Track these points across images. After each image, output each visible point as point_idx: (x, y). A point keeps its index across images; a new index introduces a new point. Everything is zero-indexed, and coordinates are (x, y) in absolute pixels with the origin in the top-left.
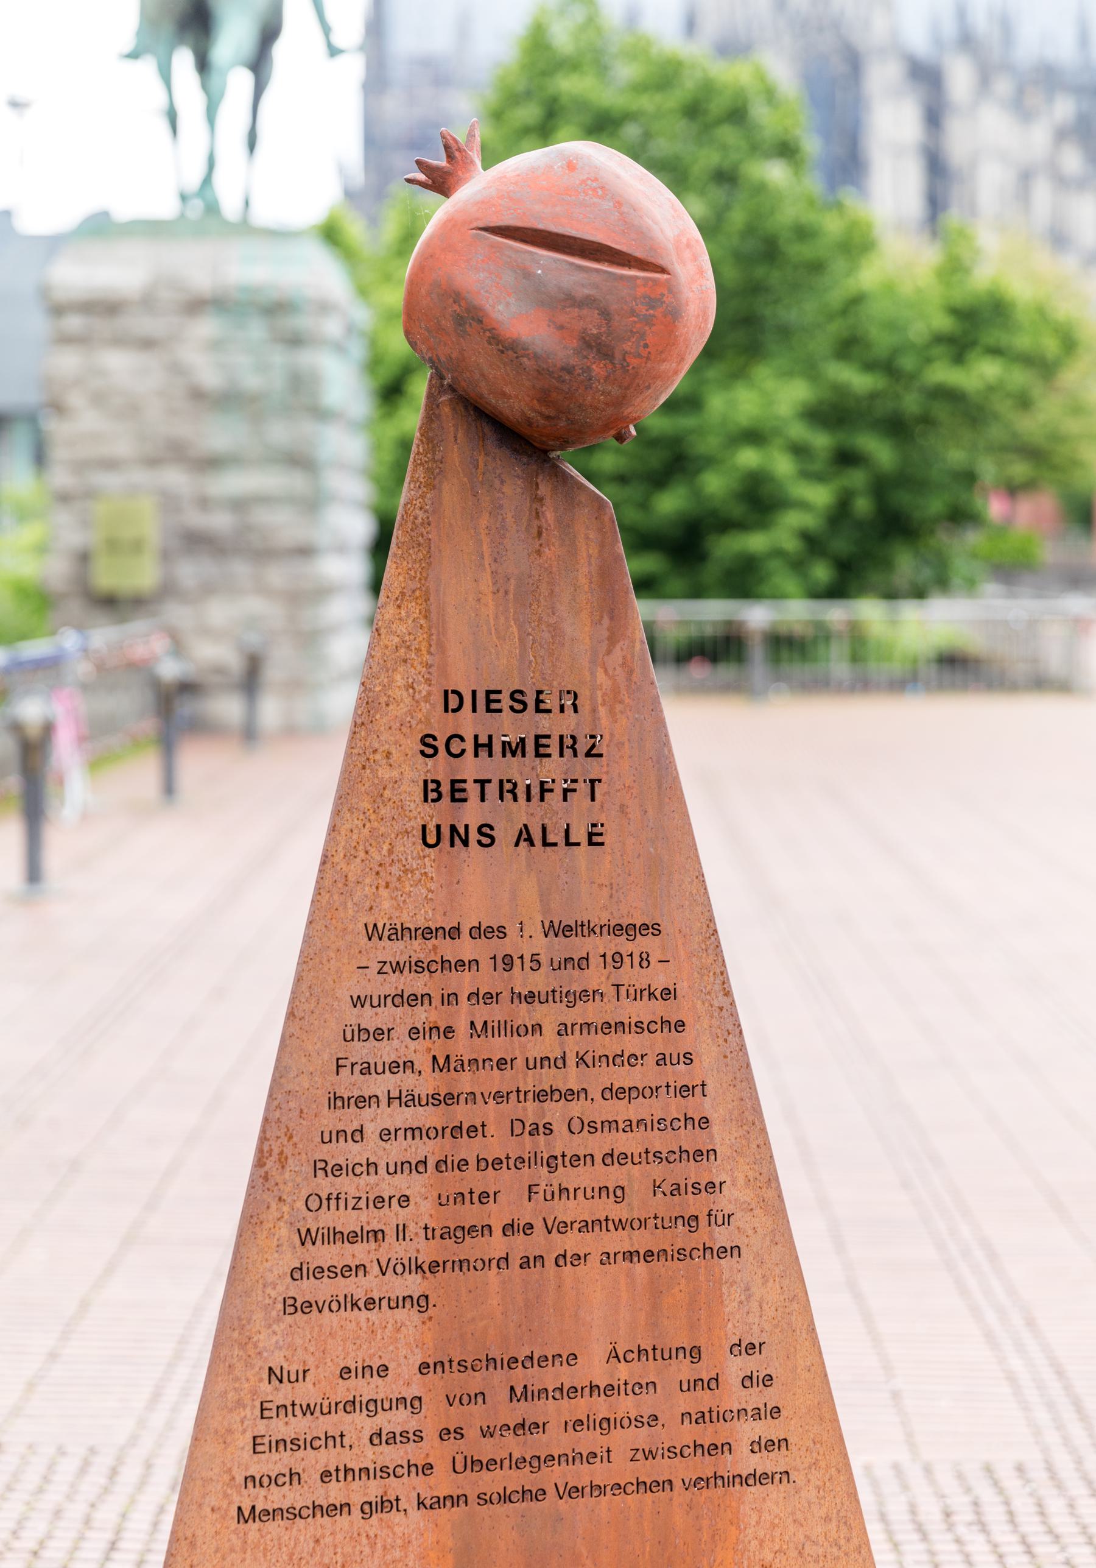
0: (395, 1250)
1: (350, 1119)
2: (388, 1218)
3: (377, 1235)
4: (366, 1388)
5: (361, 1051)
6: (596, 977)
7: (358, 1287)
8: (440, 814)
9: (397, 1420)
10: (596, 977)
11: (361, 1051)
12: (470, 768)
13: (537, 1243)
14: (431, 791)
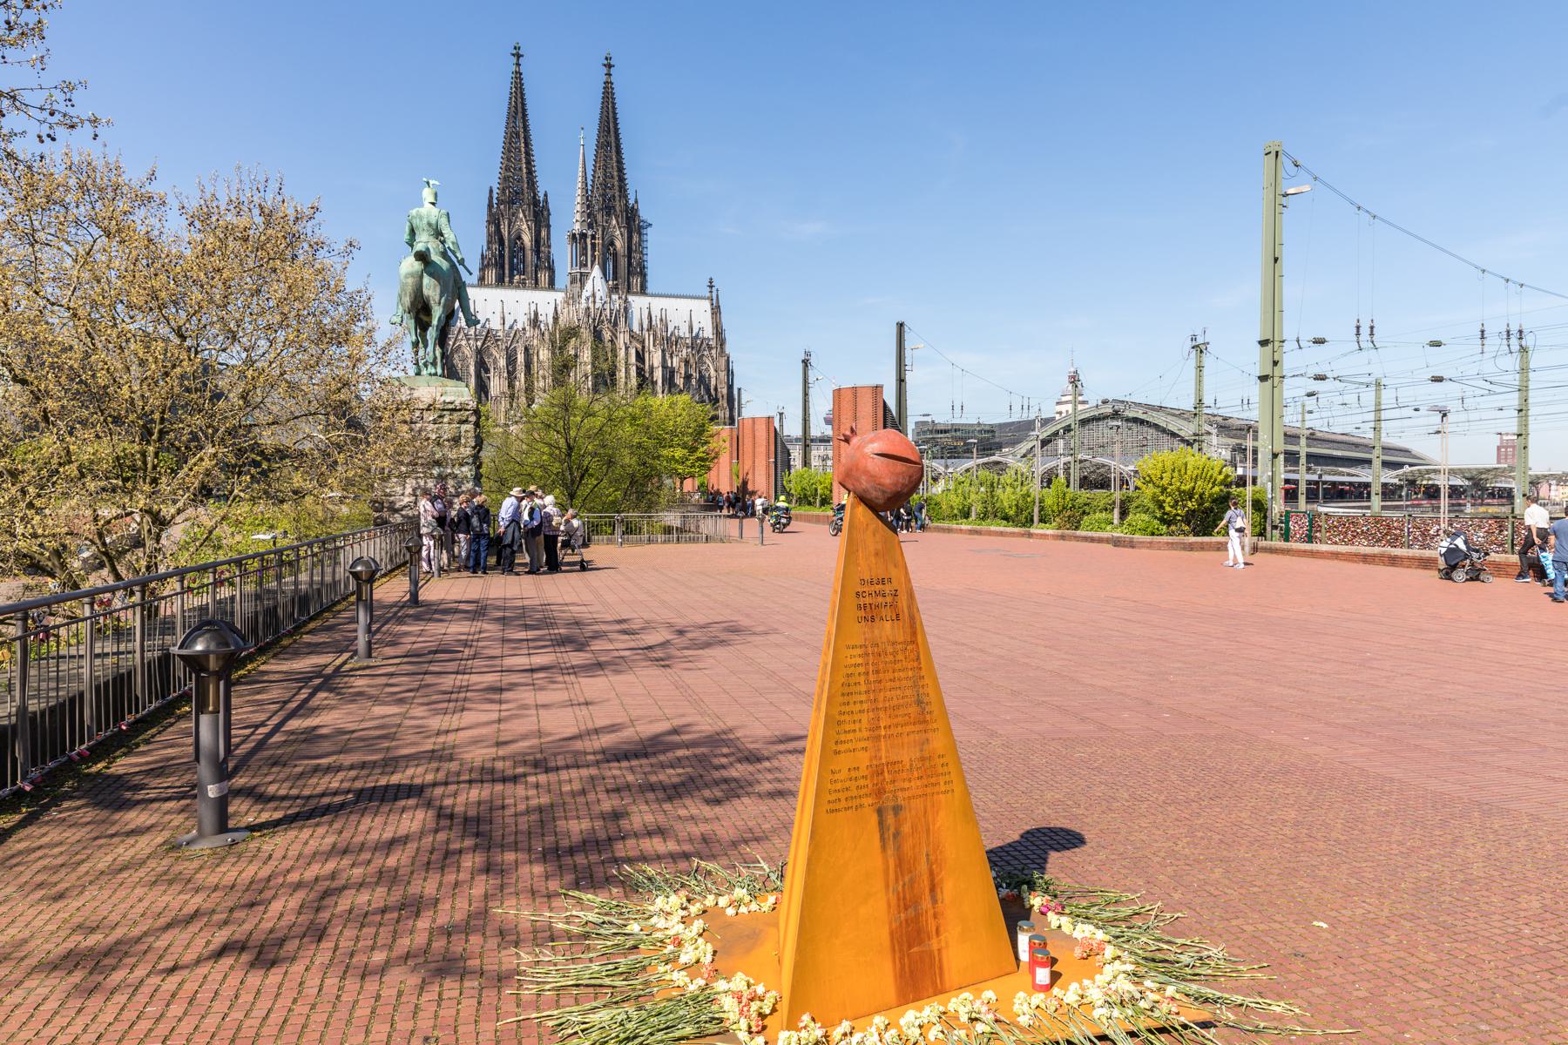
0: (858, 735)
1: (846, 699)
2: (857, 726)
3: (854, 731)
4: (853, 774)
5: (843, 709)
6: (900, 657)
7: (850, 746)
8: (862, 613)
9: (862, 782)
10: (900, 657)
11: (843, 709)
12: (868, 600)
13: (893, 731)
14: (859, 607)
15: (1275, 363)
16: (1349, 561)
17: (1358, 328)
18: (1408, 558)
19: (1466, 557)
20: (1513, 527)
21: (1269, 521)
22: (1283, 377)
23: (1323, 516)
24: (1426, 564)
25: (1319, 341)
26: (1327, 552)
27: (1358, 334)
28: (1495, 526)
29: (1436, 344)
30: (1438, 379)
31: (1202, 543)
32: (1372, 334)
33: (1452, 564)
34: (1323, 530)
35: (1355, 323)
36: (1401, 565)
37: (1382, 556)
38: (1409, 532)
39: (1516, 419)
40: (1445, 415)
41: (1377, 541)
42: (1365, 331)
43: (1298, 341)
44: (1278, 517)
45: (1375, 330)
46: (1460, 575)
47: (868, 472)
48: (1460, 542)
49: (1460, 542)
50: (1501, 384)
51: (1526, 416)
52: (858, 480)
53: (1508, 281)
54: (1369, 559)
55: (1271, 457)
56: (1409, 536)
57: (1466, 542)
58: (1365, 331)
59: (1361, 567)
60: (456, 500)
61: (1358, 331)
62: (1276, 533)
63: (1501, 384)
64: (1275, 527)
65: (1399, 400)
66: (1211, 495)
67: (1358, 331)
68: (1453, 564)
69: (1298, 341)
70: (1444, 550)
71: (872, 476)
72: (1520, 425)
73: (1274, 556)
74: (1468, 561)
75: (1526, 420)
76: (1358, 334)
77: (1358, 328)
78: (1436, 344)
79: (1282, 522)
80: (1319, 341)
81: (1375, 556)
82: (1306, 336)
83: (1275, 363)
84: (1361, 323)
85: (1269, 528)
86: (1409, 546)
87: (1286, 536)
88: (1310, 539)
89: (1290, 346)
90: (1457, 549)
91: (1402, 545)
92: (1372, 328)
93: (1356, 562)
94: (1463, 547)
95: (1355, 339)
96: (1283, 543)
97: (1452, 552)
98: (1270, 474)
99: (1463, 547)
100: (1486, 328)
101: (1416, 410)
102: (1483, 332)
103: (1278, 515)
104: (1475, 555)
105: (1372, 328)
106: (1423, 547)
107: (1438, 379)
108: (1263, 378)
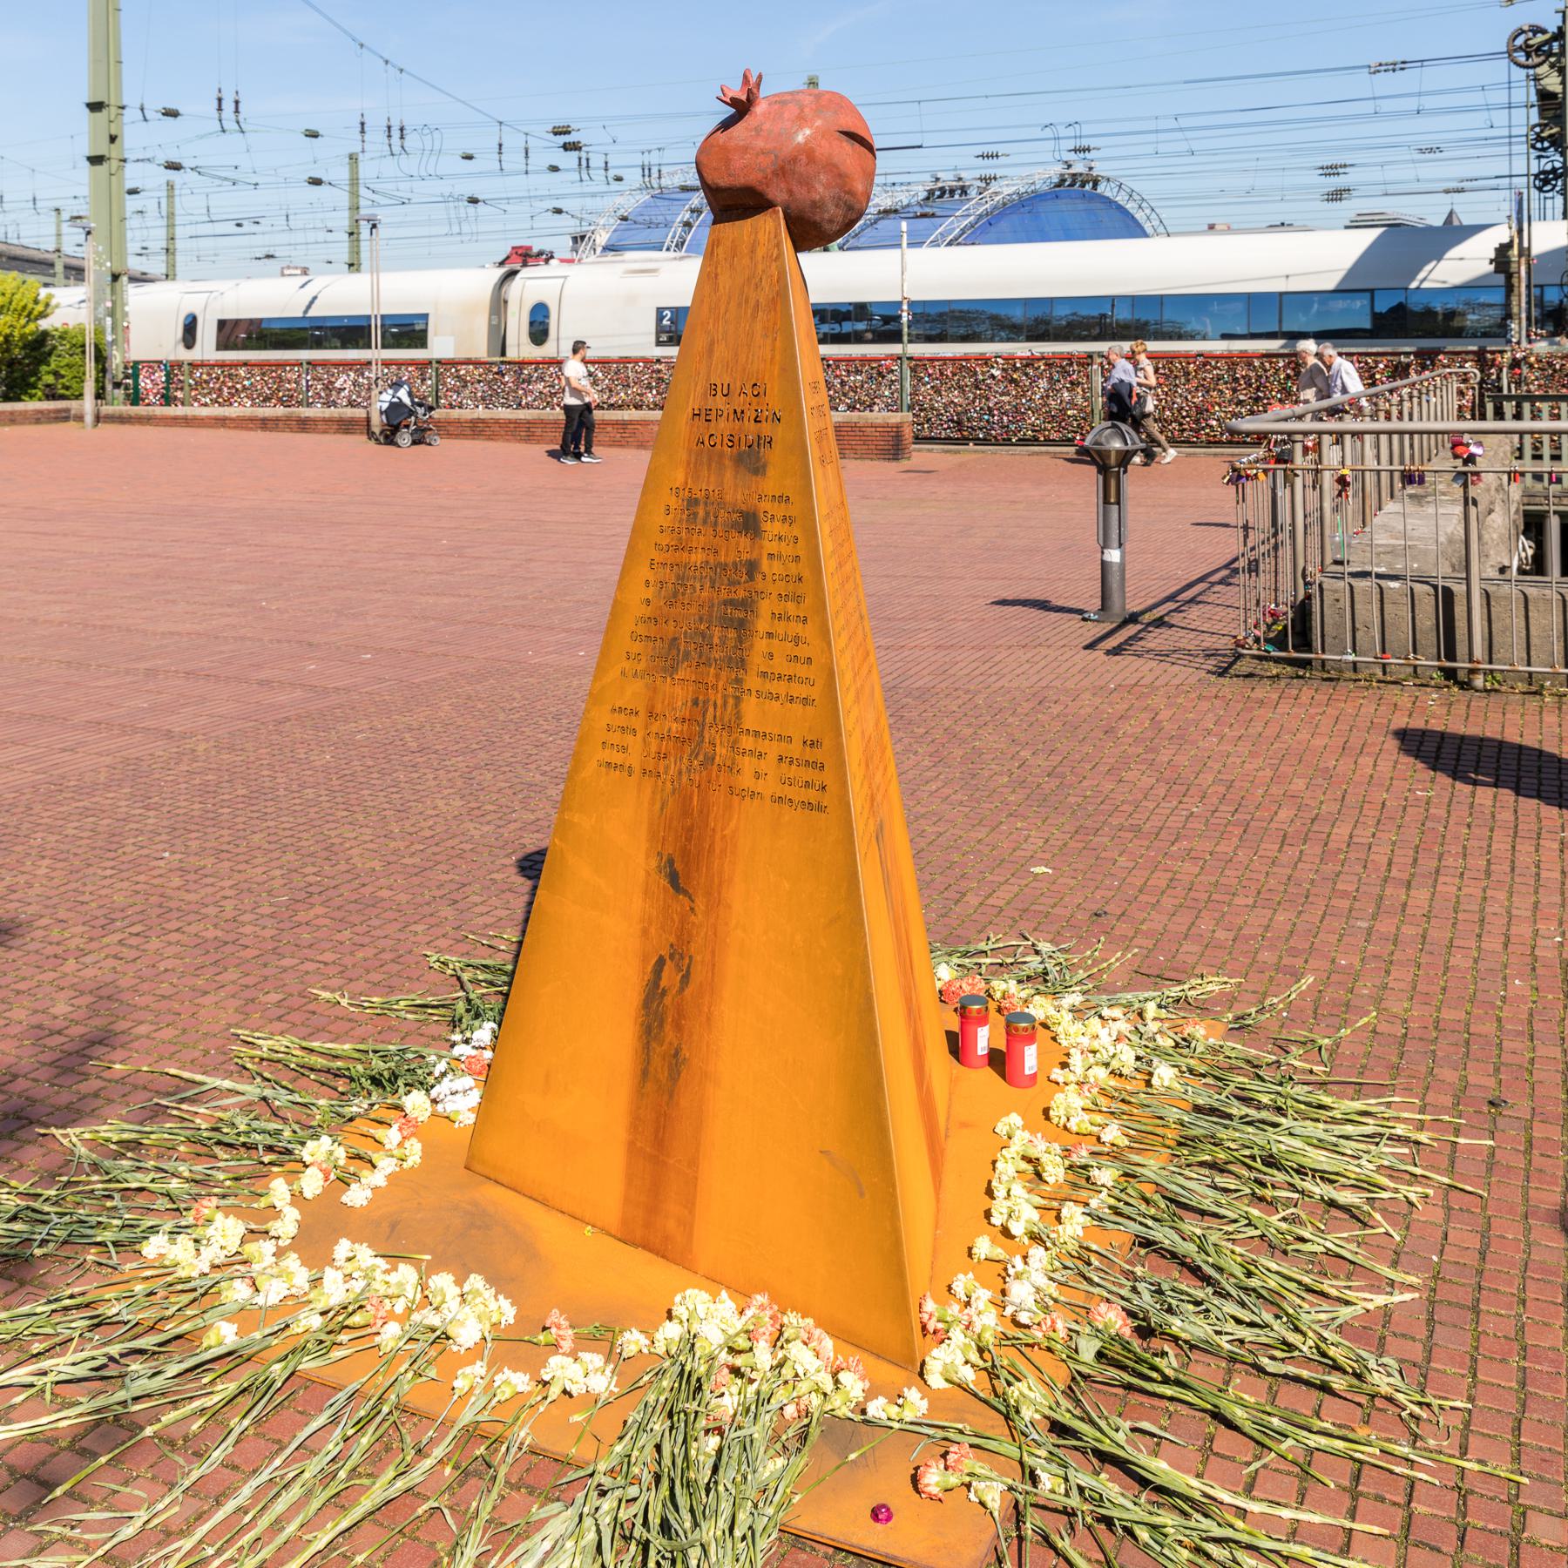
15: (113, 139)
16: (242, 428)
17: (220, 100)
18: (325, 420)
19: (412, 413)
20: (437, 376)
21: (108, 376)
22: (124, 161)
23: (186, 367)
24: (525, 432)
25: (172, 113)
26: (209, 418)
27: (220, 109)
28: (416, 374)
29: (313, 135)
30: (316, 182)
31: (12, 413)
32: (237, 111)
33: (394, 426)
34: (187, 388)
35: (215, 95)
36: (315, 431)
37: (288, 419)
38: (308, 386)
39: (347, 244)
40: (374, 226)
41: (264, 401)
42: (228, 106)
43: (142, 109)
44: (121, 369)
45: (240, 105)
46: (404, 438)
47: (835, 166)
48: (403, 394)
49: (403, 394)
50: (384, 194)
51: (358, 240)
52: (807, 183)
53: (387, 62)
54: (321, 426)
55: (109, 279)
56: (308, 391)
57: (410, 394)
58: (228, 106)
59: (259, 437)
60: (1118, 375)
61: (237, 108)
62: (120, 393)
63: (384, 194)
64: (117, 385)
65: (212, 210)
66: (23, 336)
67: (237, 108)
68: (395, 423)
69: (142, 109)
70: (385, 406)
71: (840, 175)
72: (351, 252)
73: (126, 428)
74: (413, 418)
75: (358, 246)
76: (220, 109)
77: (220, 100)
78: (313, 135)
79: (127, 377)
80: (172, 113)
81: (277, 419)
82: (154, 106)
83: (113, 139)
84: (224, 95)
85: (109, 387)
86: (309, 405)
87: (135, 398)
88: (167, 400)
89: (131, 114)
90: (401, 404)
91: (300, 403)
92: (237, 102)
93: (251, 429)
94: (407, 400)
95: (217, 115)
96: (129, 407)
97: (395, 408)
98: (109, 304)
99: (407, 400)
100: (366, 119)
101: (239, 225)
102: (363, 124)
103: (121, 366)
104: (421, 411)
105: (237, 102)
106: (327, 404)
107: (316, 182)
108: (96, 160)
